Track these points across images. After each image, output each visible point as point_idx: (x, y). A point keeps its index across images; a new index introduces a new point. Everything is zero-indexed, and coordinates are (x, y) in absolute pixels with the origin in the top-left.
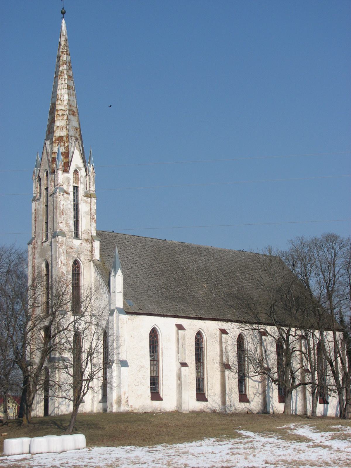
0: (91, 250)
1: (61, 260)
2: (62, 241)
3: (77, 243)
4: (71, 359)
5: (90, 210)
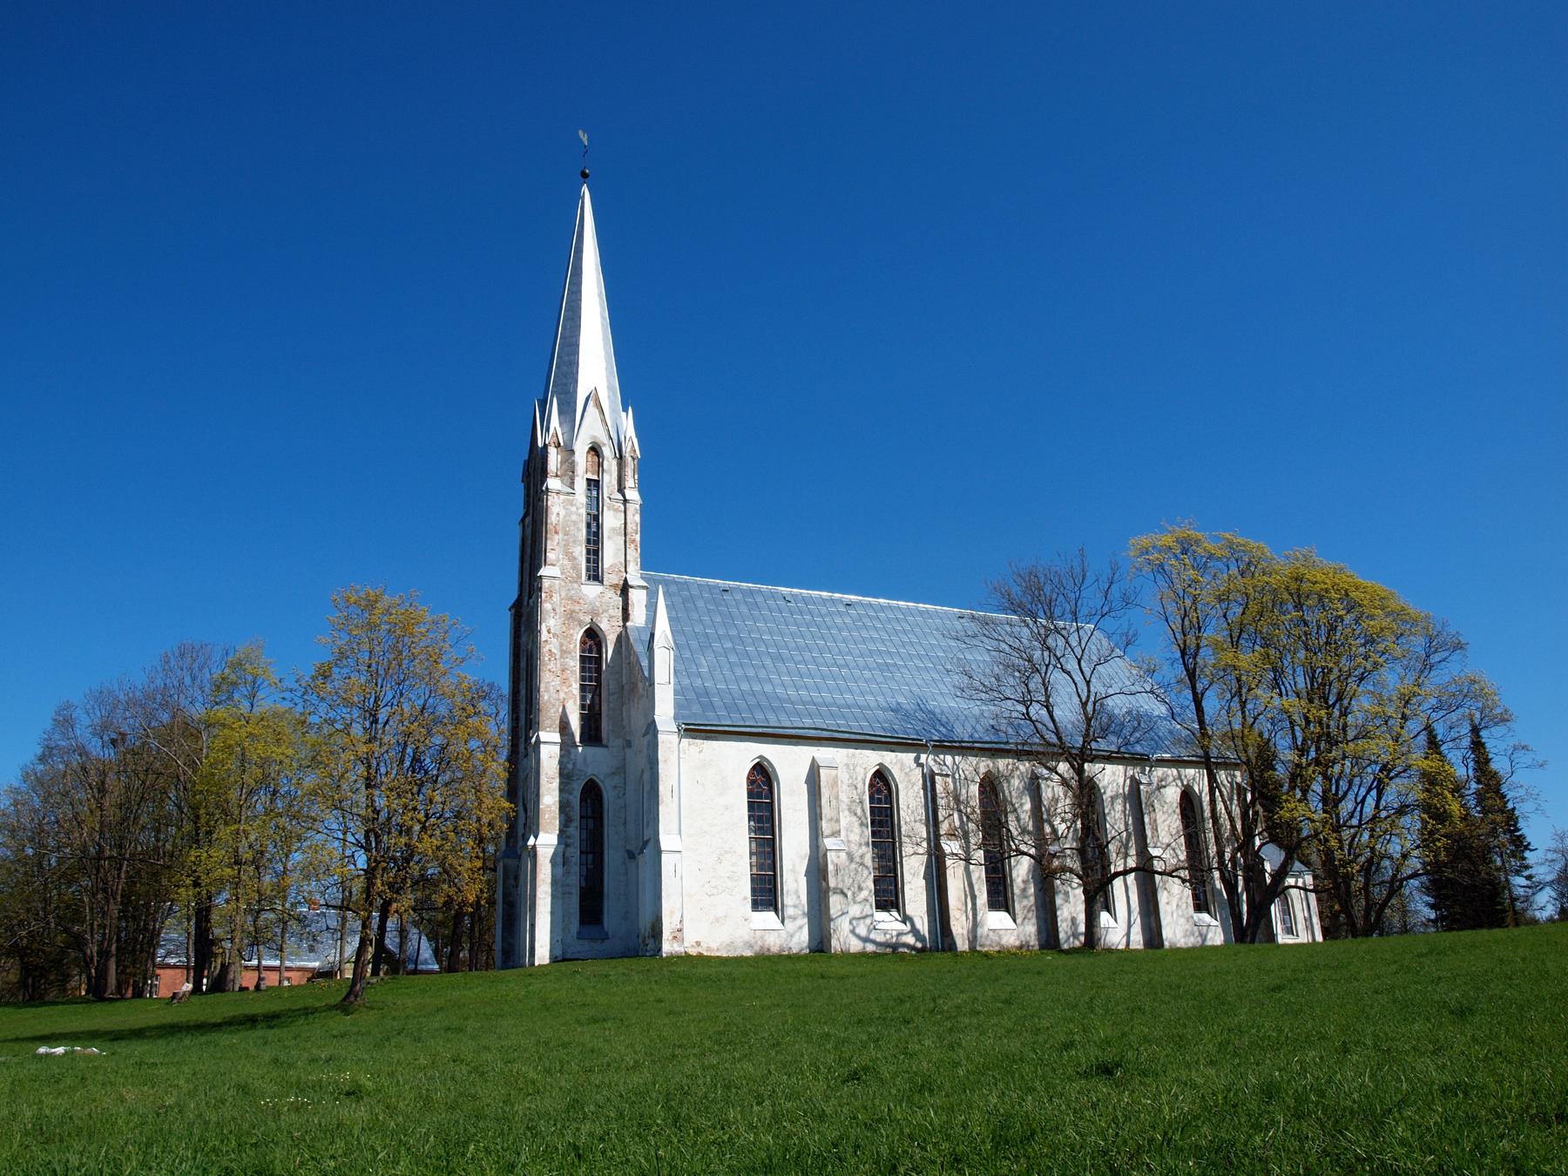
2: (550, 586)
3: (592, 591)
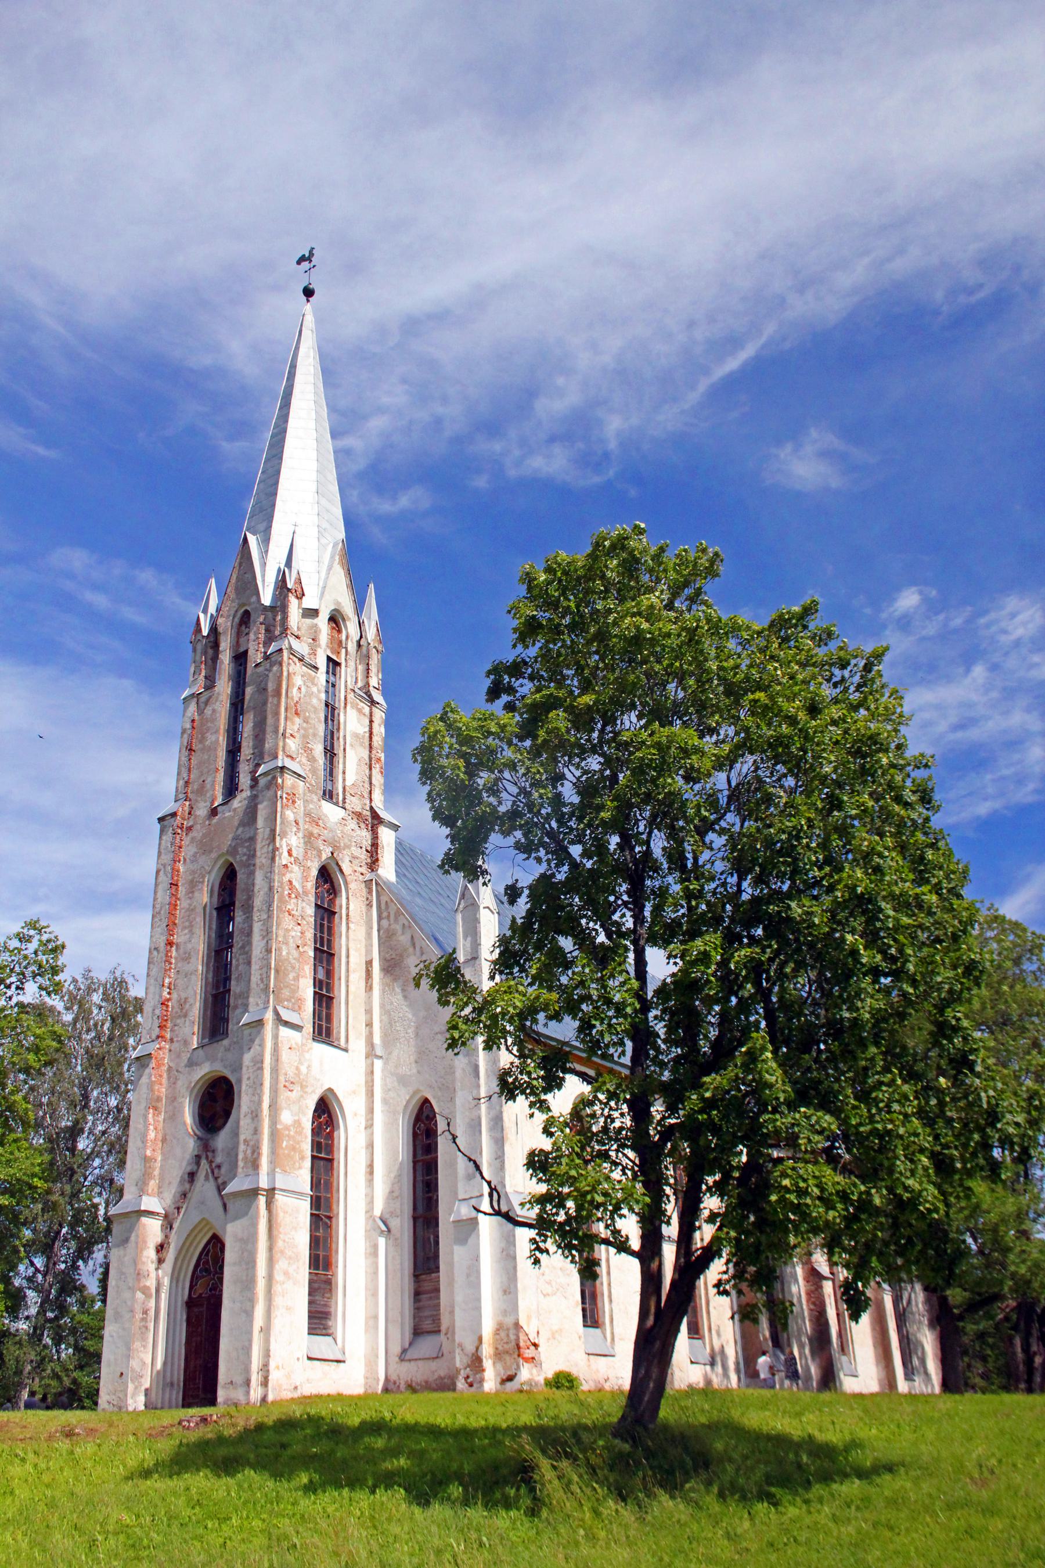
0: (369, 849)
1: (288, 845)
3: (331, 812)
4: (225, 445)
5: (367, 735)
